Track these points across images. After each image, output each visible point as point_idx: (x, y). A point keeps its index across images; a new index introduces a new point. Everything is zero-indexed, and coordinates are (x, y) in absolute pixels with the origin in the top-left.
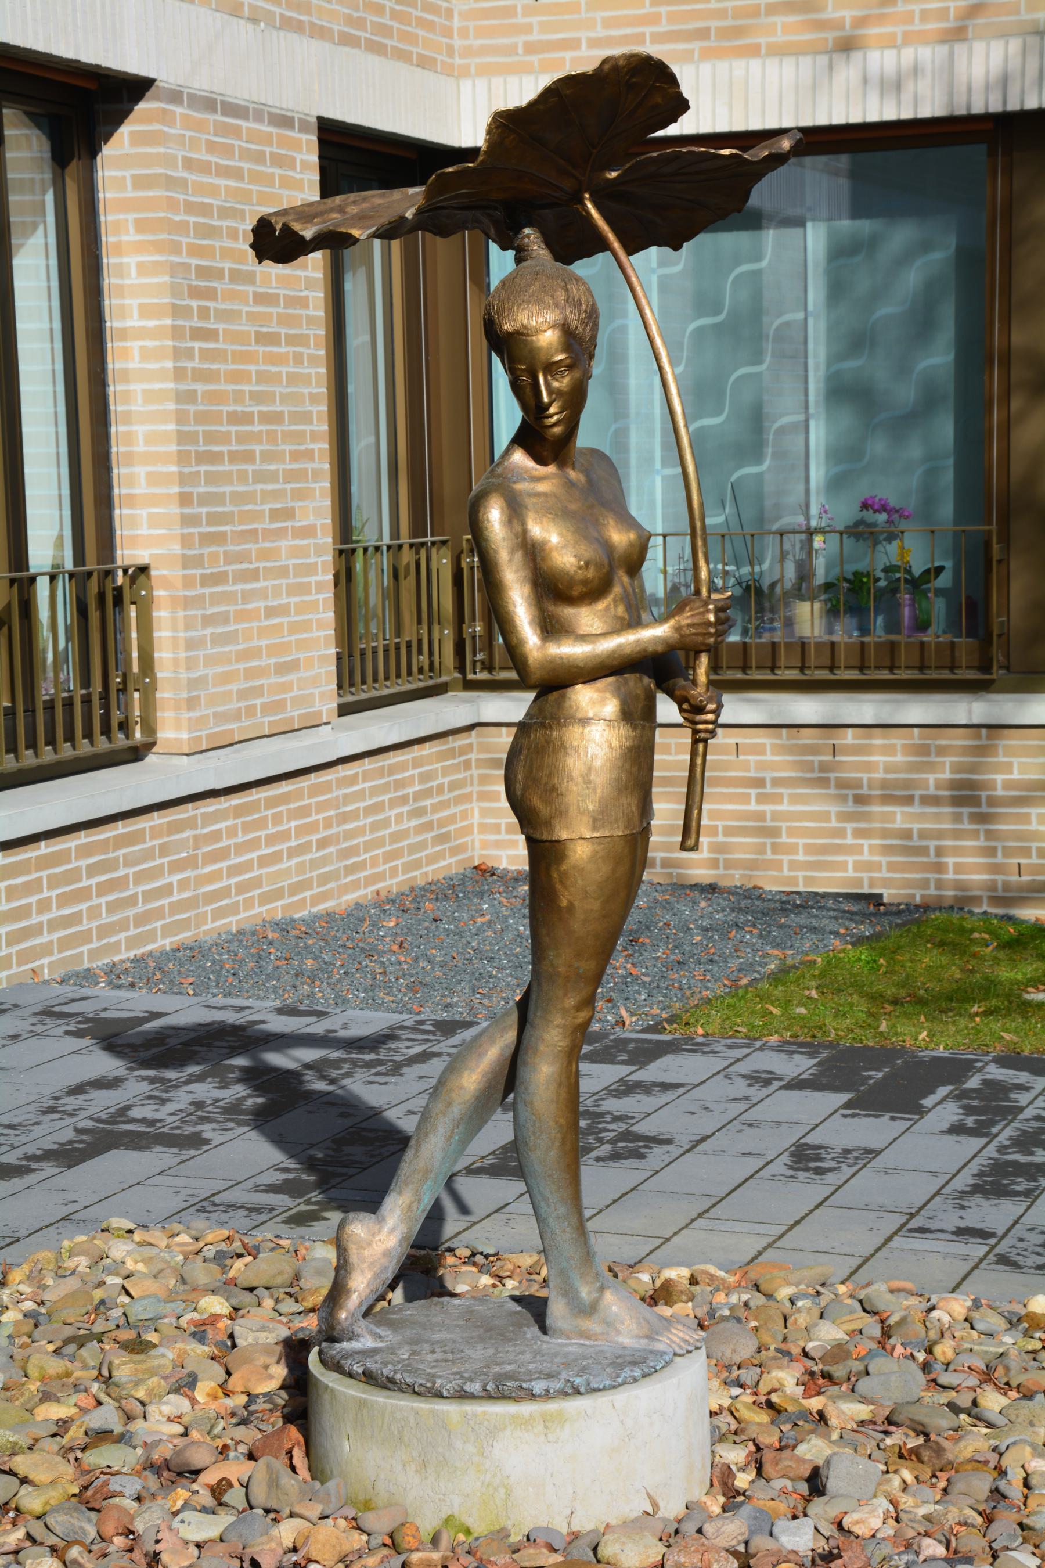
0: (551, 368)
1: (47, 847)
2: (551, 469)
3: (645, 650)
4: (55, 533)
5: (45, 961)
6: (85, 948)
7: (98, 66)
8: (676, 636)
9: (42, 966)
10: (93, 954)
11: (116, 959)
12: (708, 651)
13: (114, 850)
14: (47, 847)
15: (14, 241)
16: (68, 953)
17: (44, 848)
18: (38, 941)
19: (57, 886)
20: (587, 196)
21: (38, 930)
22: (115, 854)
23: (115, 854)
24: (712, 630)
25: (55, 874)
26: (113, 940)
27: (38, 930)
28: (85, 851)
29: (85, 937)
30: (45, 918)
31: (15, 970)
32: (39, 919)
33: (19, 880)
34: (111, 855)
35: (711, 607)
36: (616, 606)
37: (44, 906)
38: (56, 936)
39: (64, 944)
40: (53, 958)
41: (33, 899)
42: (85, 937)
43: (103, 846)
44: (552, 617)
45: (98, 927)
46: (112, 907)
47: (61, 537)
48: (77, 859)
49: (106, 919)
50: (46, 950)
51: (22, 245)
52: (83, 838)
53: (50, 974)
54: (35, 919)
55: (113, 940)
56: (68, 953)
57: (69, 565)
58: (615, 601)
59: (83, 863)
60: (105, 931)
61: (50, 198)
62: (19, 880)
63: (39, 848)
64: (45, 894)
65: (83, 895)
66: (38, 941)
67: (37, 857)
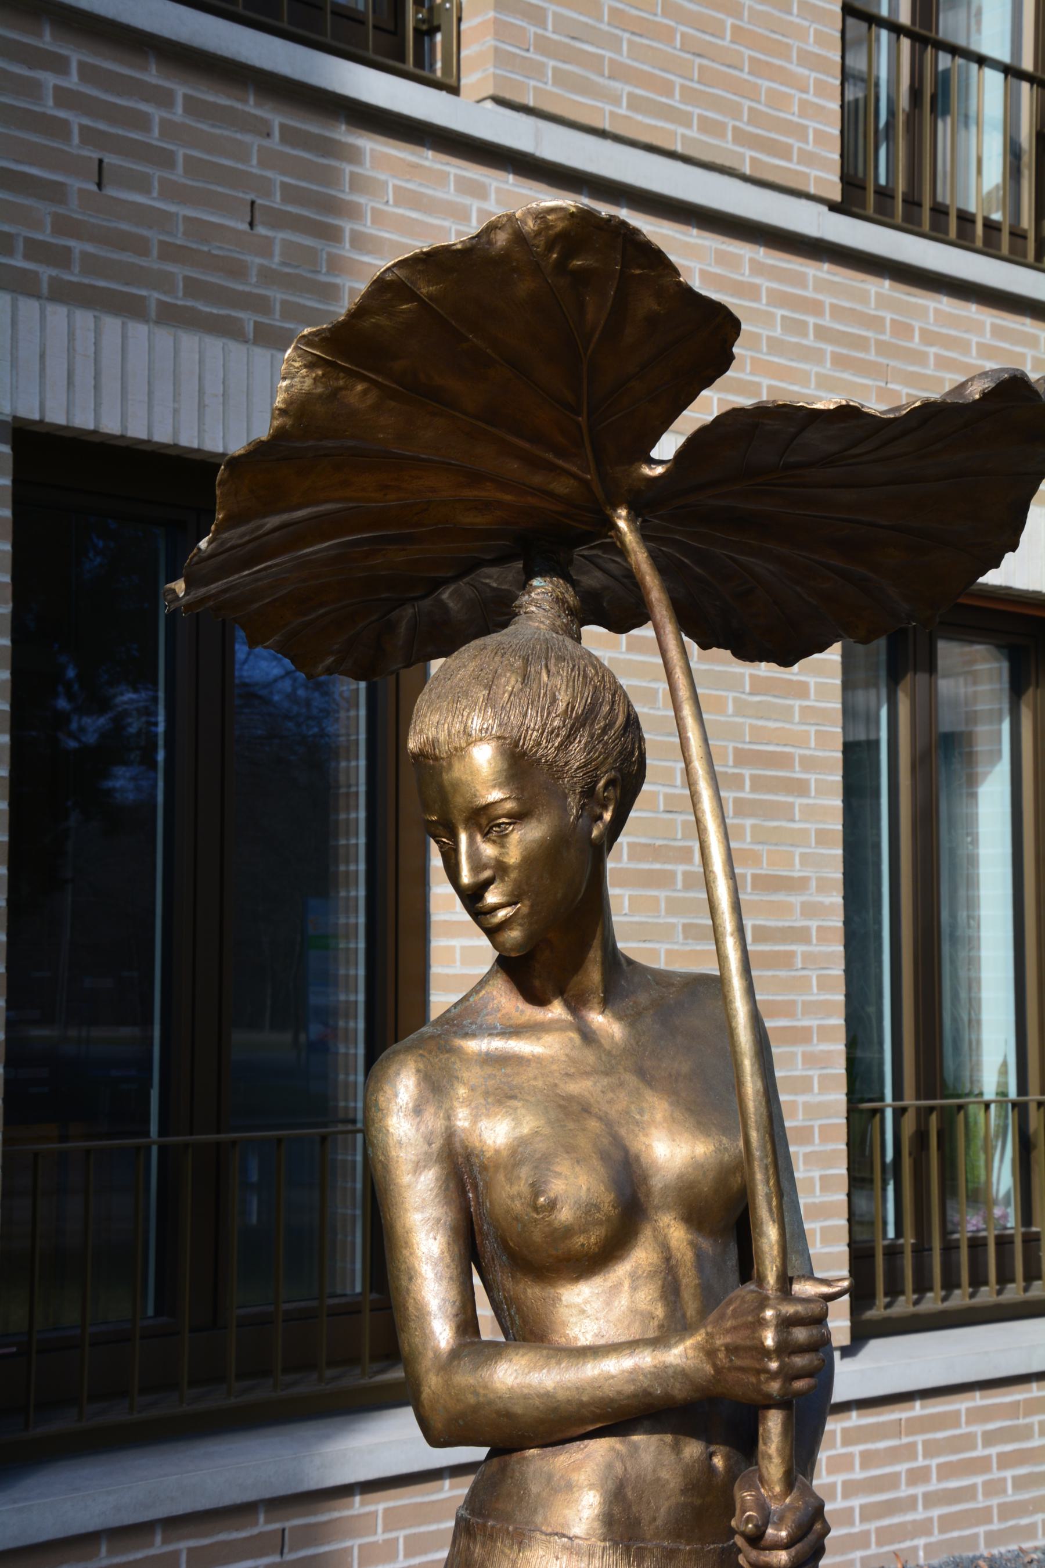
0: (483, 821)
1: (922, 1407)
2: (557, 1010)
3: (647, 1393)
4: (1000, 1059)
5: (921, 1542)
6: (981, 1530)
7: (1010, 588)
8: (709, 1369)
9: (915, 1549)
10: (992, 1538)
11: (1027, 1545)
12: (778, 1405)
13: (1026, 1415)
14: (451, 1488)
15: (980, 770)
16: (955, 1534)
17: (918, 1409)
18: (909, 1517)
19: (938, 1454)
20: (623, 512)
21: (910, 1503)
22: (1028, 1420)
23: (1028, 1420)
24: (774, 1365)
25: (936, 1440)
26: (1024, 1521)
27: (910, 1503)
28: (977, 1415)
29: (983, 1516)
30: (919, 1490)
31: (873, 1550)
32: (911, 1491)
33: (882, 1445)
34: (1021, 1421)
35: (769, 1314)
36: (634, 1289)
37: (918, 1476)
38: (936, 1513)
39: (947, 1523)
40: (933, 1539)
41: (902, 1468)
42: (983, 1516)
43: (896, 1429)
44: (511, 1301)
45: (999, 1505)
46: (1020, 1483)
47: (1005, 1064)
48: (968, 1423)
49: (1011, 1496)
50: (922, 1528)
51: (989, 773)
52: (978, 1399)
53: (926, 1559)
54: (904, 1491)
55: (1024, 1521)
56: (955, 1534)
57: (1013, 1093)
58: (634, 1277)
59: (978, 1429)
60: (1007, 1511)
61: (1006, 726)
62: (882, 1445)
63: (913, 1408)
64: (921, 1462)
65: (981, 1465)
66: (909, 1517)
67: (908, 1420)
